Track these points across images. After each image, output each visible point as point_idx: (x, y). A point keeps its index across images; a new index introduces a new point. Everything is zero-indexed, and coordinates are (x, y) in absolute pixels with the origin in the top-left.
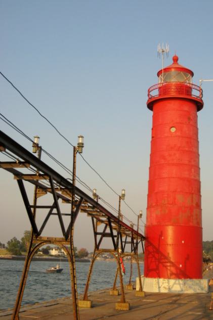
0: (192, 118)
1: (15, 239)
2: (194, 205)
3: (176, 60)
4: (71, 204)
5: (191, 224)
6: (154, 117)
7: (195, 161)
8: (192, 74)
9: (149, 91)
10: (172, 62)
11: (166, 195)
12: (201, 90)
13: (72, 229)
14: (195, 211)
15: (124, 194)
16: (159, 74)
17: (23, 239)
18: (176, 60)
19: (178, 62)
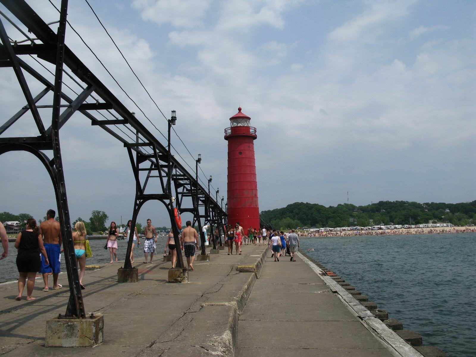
2: (254, 195)
3: (240, 110)
5: (252, 206)
7: (253, 171)
8: (249, 119)
9: (225, 131)
17: (91, 219)
18: (240, 110)
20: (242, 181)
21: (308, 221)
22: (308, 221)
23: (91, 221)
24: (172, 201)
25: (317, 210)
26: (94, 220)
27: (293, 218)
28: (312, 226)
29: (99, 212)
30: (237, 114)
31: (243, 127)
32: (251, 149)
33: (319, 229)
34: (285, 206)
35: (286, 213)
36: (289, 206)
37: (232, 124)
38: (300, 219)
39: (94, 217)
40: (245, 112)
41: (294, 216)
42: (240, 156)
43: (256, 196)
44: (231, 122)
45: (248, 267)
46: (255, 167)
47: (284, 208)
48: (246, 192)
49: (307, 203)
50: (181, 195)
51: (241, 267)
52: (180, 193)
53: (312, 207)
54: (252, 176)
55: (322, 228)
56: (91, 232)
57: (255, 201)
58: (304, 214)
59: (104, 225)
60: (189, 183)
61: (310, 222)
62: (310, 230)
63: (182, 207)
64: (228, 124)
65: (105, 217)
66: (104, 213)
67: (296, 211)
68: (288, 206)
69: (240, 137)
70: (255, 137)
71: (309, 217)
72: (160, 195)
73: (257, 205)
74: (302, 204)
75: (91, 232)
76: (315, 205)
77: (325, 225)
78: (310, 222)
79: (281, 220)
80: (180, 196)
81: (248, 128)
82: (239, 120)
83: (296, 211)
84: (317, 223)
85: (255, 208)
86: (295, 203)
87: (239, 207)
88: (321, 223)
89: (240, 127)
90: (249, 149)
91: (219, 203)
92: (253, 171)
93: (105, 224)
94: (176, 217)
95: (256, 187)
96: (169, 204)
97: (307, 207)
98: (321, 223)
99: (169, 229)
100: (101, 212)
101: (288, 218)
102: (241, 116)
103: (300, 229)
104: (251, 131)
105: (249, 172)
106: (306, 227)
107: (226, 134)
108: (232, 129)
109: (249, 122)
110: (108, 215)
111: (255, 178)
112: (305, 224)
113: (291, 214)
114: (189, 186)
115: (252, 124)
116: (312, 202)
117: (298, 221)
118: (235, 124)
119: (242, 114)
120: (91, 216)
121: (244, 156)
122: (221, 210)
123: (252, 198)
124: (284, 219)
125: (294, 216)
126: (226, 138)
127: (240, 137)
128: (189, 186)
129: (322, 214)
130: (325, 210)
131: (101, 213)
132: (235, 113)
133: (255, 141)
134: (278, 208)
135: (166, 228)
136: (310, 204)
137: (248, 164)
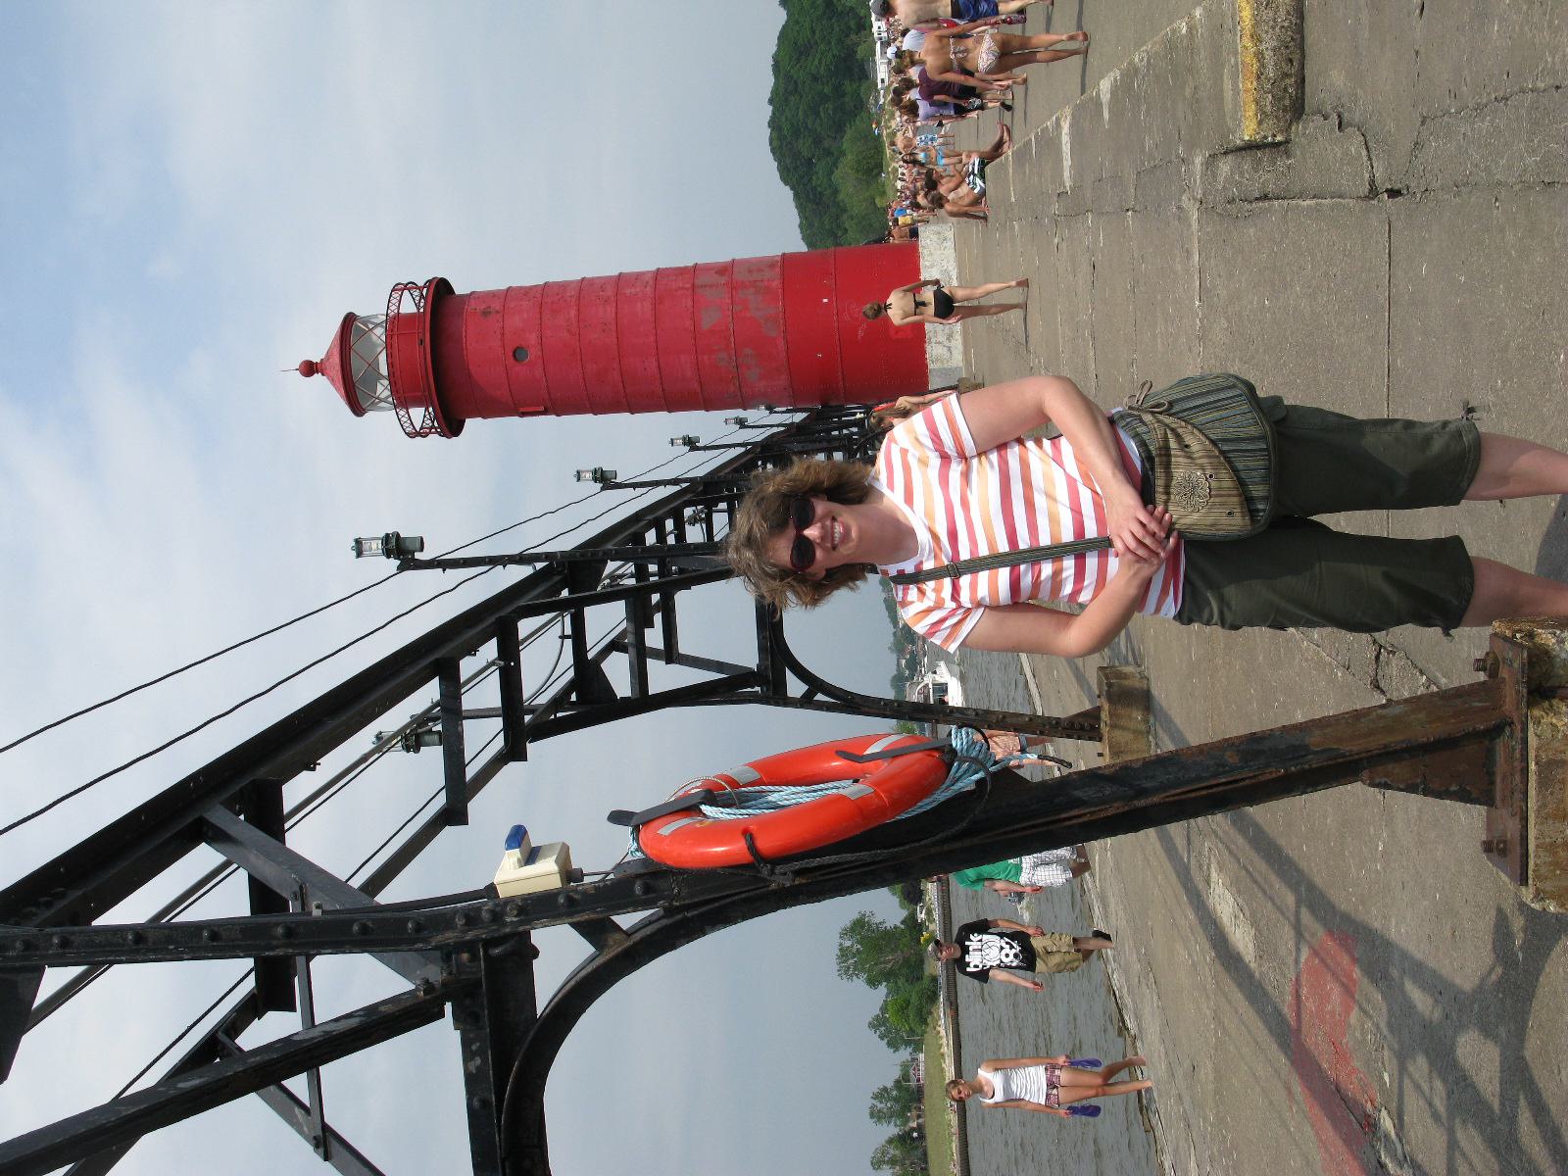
0: (483, 306)
1: (877, 1023)
2: (723, 280)
3: (309, 369)
4: (587, 610)
5: (776, 284)
6: (485, 414)
7: (602, 289)
8: (349, 320)
9: (415, 434)
10: (317, 377)
11: (706, 357)
12: (400, 288)
13: (1014, 647)
14: (740, 275)
15: (684, 438)
16: (358, 409)
17: (873, 982)
18: (309, 369)
19: (316, 359)
20: (652, 338)
21: (844, 94)
22: (844, 94)
23: (880, 983)
24: (555, 883)
25: (798, 60)
26: (877, 969)
27: (834, 157)
28: (867, 77)
29: (844, 954)
30: (333, 381)
31: (388, 346)
32: (497, 305)
33: (878, 45)
34: (787, 194)
35: (814, 189)
36: (787, 174)
37: (383, 404)
38: (839, 129)
39: (863, 970)
40: (320, 344)
41: (829, 153)
42: (532, 354)
43: (725, 269)
44: (374, 406)
45: (1256, 38)
46: (583, 279)
47: (797, 196)
48: (709, 319)
49: (771, 101)
50: (654, 666)
51: (1251, 110)
52: (640, 676)
53: (788, 78)
54: (628, 291)
55: (875, 30)
56: (926, 982)
57: (750, 271)
58: (819, 112)
59: (896, 927)
60: (568, 619)
61: (848, 87)
62: (883, 81)
63: (746, 654)
64: (383, 421)
65: (863, 927)
66: (847, 933)
67: (804, 146)
68: (785, 179)
69: (441, 360)
70: (441, 288)
71: (827, 90)
72: (481, 1053)
73: (769, 263)
74: (773, 124)
75: (926, 982)
76: (777, 68)
77: (861, 18)
78: (848, 87)
79: (844, 210)
80: (663, 677)
81: (397, 324)
82: (358, 367)
83: (804, 146)
84: (851, 53)
85: (783, 274)
86: (773, 151)
87: (781, 344)
88: (853, 37)
89: (390, 365)
90: (497, 312)
91: (757, 436)
92: (602, 289)
93: (889, 925)
94: (766, 843)
95: (681, 271)
96: (595, 931)
97: (786, 99)
98: (853, 37)
99: (898, 664)
100: (841, 944)
101: (837, 173)
102: (336, 359)
103: (878, 124)
104: (408, 306)
105: (610, 310)
106: (872, 100)
107: (431, 428)
108: (403, 399)
109: (366, 321)
110: (856, 916)
111: (638, 276)
112: (860, 105)
113: (820, 168)
114: (591, 613)
115: (373, 306)
116: (767, 81)
117: (848, 136)
118: (383, 389)
119: (329, 354)
120: (860, 984)
121: (532, 338)
122: (793, 430)
123: (734, 287)
124: (841, 196)
125: (829, 153)
126: (451, 427)
127: (441, 360)
128: (591, 613)
129: (814, 33)
130: (797, 22)
131: (848, 943)
132: (324, 391)
133: (460, 289)
134: (797, 220)
135: (894, 677)
136: (775, 92)
137: (573, 313)
